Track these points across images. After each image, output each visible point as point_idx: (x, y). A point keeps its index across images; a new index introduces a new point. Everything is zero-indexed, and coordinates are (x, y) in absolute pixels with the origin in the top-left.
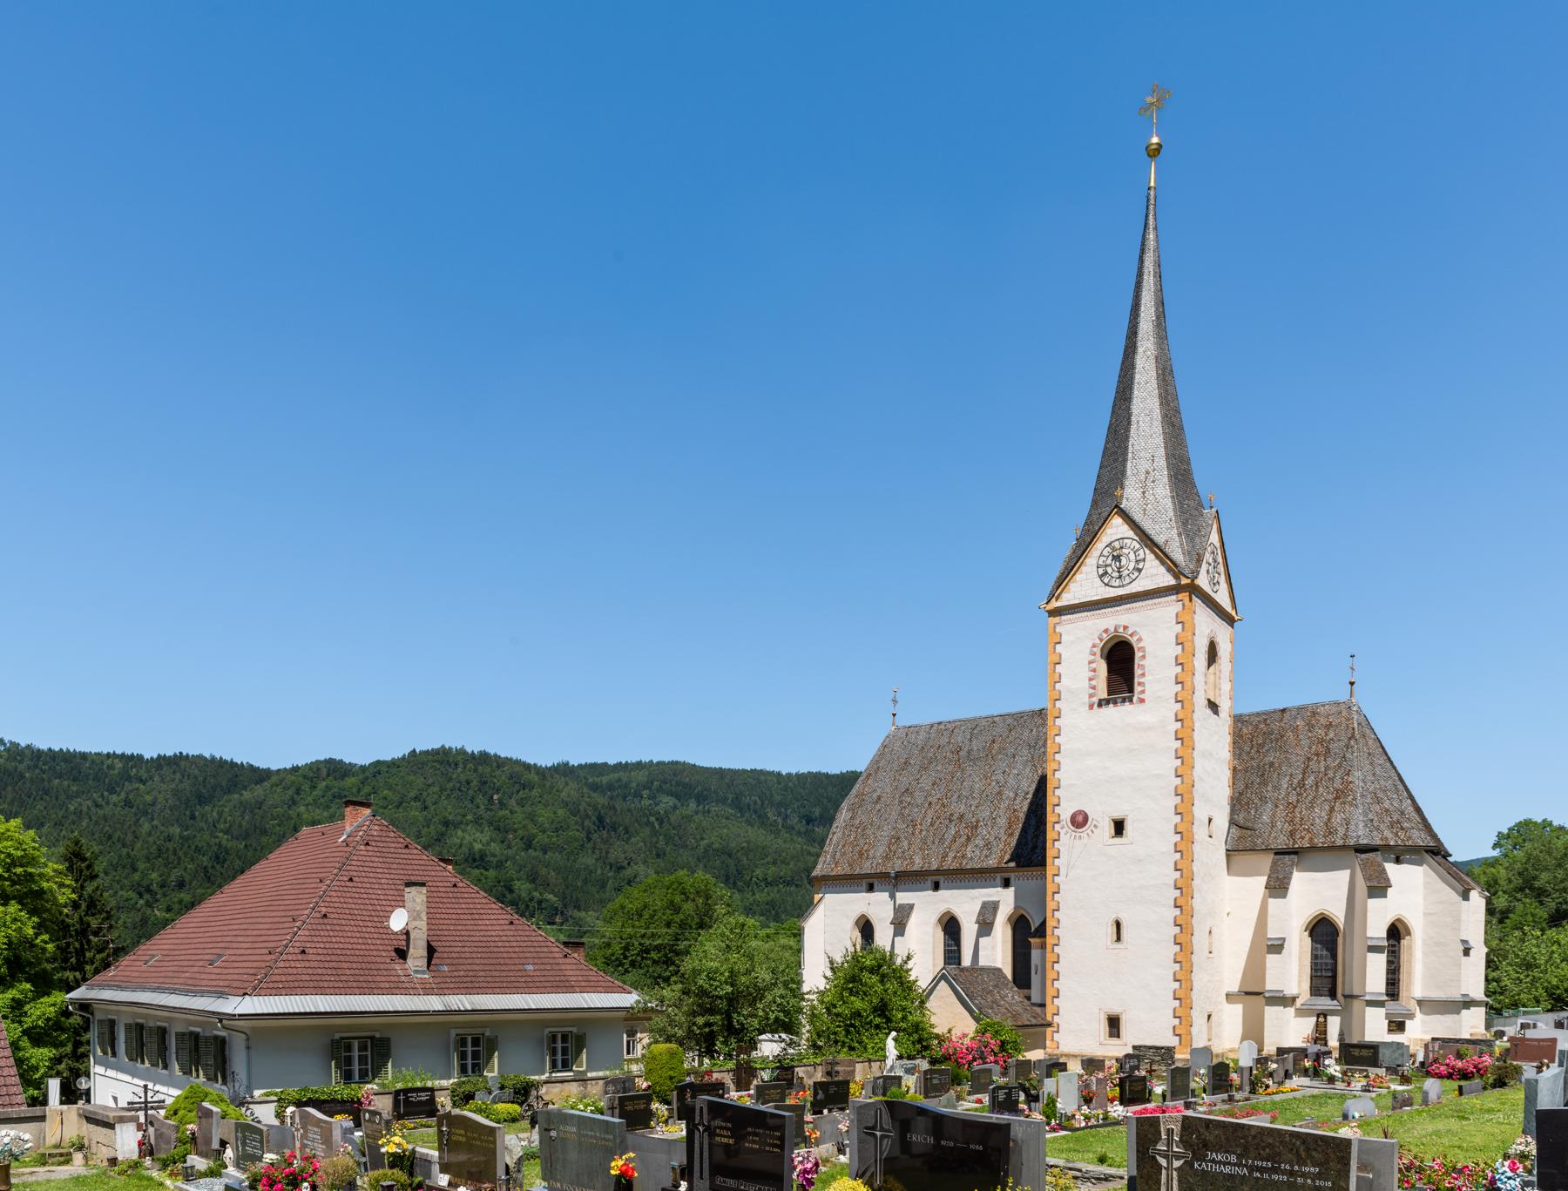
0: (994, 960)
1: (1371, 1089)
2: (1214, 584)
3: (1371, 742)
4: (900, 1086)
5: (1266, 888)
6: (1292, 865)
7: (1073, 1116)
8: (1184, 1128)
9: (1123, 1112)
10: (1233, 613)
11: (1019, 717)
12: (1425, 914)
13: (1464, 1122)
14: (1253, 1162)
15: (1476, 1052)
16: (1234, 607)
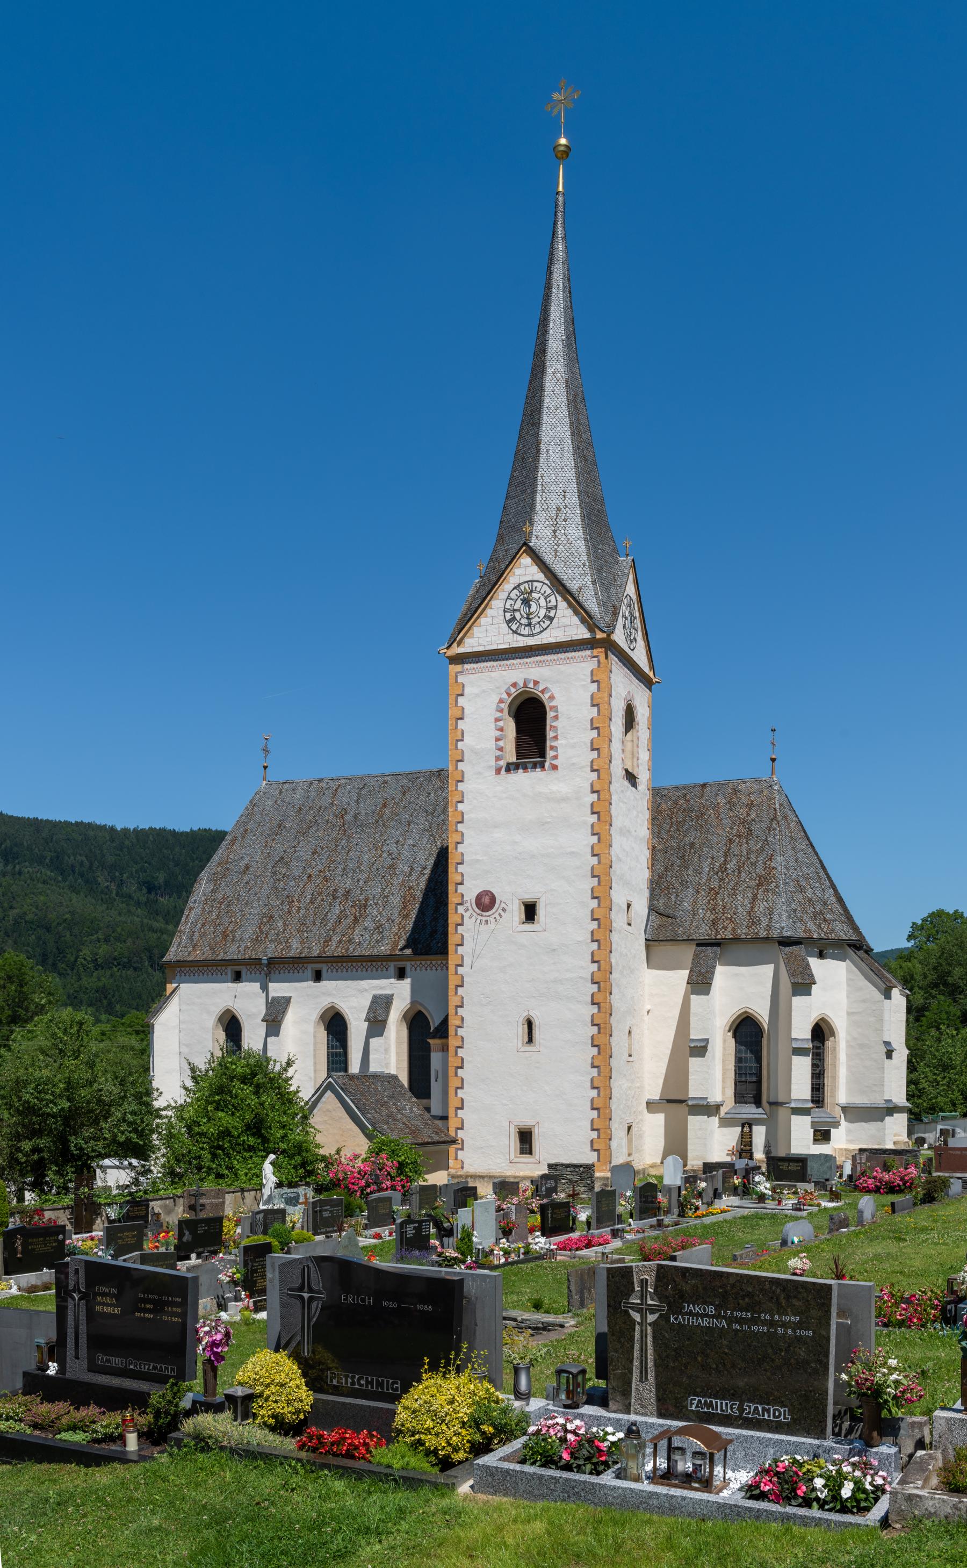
0: (387, 1065)
1: (802, 1207)
2: (631, 641)
3: (792, 825)
4: (284, 1221)
5: (688, 983)
6: (715, 959)
7: (492, 1251)
8: (658, 1278)
9: (545, 1244)
10: (651, 674)
11: (414, 777)
12: (849, 1014)
13: (901, 1244)
14: (732, 1313)
15: (902, 1163)
16: (652, 668)
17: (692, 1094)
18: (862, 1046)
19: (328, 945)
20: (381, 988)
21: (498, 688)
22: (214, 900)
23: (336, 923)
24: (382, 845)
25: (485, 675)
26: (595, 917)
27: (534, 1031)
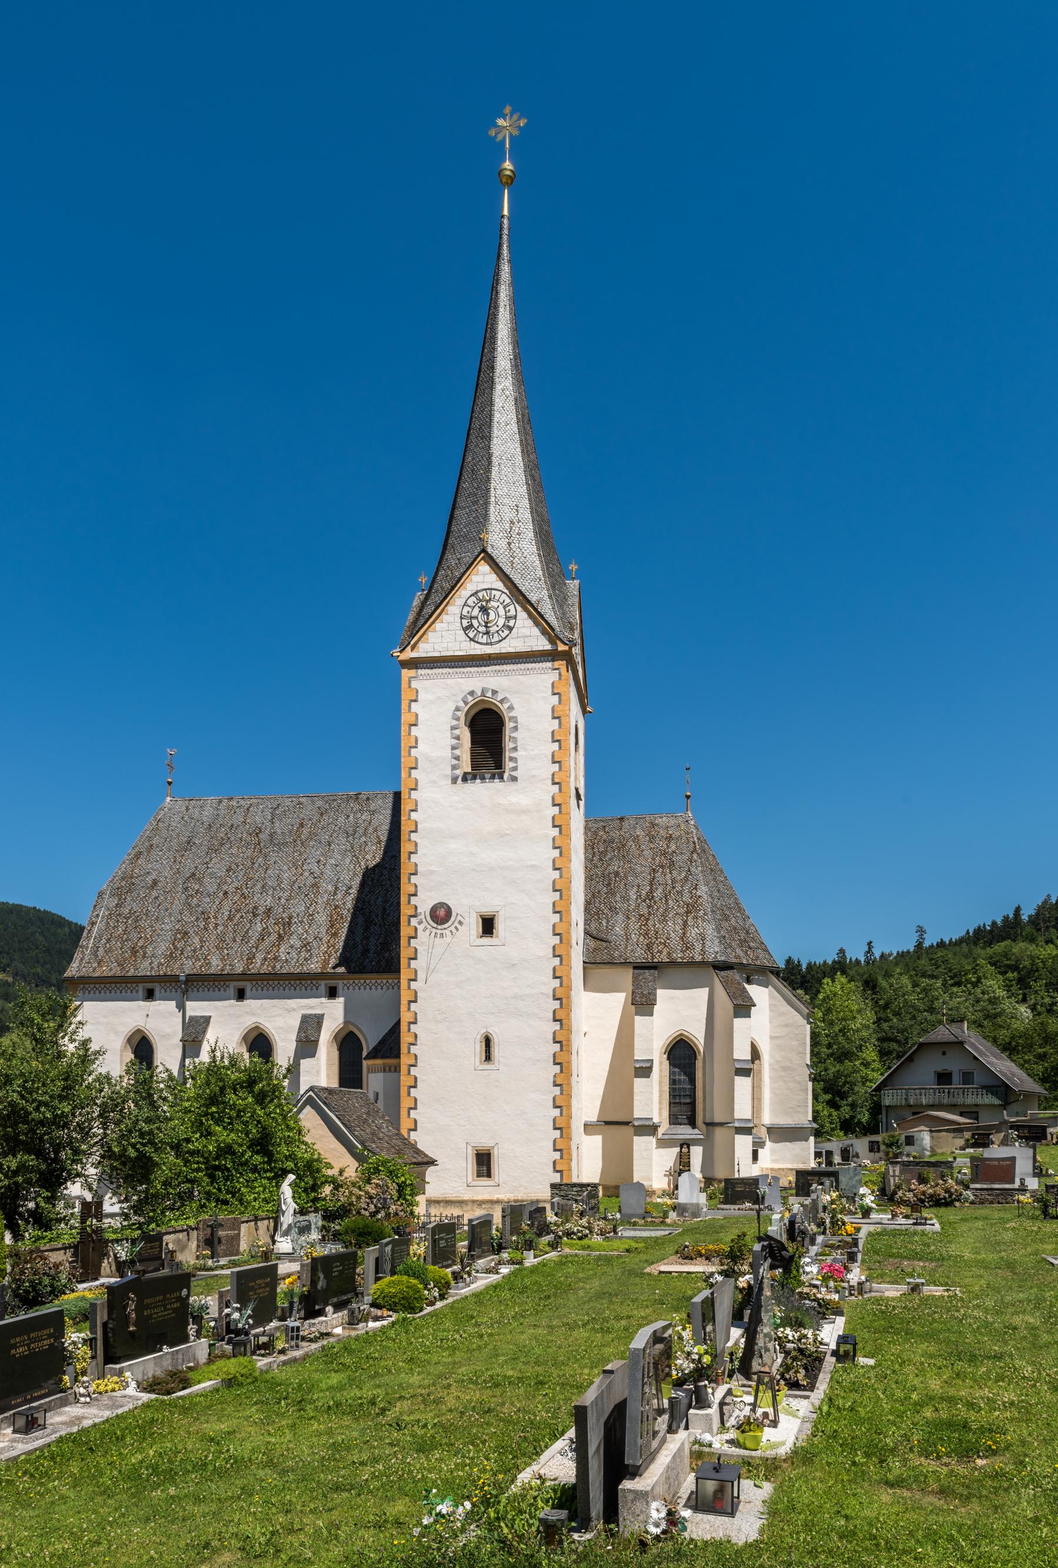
12: (771, 1038)
17: (638, 1114)
18: (785, 1069)
19: (252, 963)
20: (311, 1008)
21: (454, 695)
22: (119, 915)
23: (258, 940)
24: (303, 864)
25: (439, 682)
26: (557, 932)
27: (492, 1049)
